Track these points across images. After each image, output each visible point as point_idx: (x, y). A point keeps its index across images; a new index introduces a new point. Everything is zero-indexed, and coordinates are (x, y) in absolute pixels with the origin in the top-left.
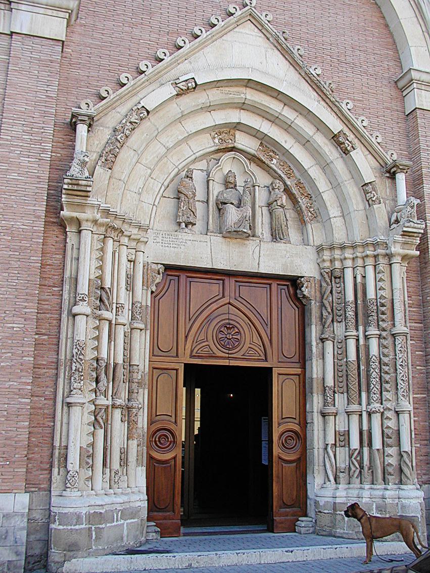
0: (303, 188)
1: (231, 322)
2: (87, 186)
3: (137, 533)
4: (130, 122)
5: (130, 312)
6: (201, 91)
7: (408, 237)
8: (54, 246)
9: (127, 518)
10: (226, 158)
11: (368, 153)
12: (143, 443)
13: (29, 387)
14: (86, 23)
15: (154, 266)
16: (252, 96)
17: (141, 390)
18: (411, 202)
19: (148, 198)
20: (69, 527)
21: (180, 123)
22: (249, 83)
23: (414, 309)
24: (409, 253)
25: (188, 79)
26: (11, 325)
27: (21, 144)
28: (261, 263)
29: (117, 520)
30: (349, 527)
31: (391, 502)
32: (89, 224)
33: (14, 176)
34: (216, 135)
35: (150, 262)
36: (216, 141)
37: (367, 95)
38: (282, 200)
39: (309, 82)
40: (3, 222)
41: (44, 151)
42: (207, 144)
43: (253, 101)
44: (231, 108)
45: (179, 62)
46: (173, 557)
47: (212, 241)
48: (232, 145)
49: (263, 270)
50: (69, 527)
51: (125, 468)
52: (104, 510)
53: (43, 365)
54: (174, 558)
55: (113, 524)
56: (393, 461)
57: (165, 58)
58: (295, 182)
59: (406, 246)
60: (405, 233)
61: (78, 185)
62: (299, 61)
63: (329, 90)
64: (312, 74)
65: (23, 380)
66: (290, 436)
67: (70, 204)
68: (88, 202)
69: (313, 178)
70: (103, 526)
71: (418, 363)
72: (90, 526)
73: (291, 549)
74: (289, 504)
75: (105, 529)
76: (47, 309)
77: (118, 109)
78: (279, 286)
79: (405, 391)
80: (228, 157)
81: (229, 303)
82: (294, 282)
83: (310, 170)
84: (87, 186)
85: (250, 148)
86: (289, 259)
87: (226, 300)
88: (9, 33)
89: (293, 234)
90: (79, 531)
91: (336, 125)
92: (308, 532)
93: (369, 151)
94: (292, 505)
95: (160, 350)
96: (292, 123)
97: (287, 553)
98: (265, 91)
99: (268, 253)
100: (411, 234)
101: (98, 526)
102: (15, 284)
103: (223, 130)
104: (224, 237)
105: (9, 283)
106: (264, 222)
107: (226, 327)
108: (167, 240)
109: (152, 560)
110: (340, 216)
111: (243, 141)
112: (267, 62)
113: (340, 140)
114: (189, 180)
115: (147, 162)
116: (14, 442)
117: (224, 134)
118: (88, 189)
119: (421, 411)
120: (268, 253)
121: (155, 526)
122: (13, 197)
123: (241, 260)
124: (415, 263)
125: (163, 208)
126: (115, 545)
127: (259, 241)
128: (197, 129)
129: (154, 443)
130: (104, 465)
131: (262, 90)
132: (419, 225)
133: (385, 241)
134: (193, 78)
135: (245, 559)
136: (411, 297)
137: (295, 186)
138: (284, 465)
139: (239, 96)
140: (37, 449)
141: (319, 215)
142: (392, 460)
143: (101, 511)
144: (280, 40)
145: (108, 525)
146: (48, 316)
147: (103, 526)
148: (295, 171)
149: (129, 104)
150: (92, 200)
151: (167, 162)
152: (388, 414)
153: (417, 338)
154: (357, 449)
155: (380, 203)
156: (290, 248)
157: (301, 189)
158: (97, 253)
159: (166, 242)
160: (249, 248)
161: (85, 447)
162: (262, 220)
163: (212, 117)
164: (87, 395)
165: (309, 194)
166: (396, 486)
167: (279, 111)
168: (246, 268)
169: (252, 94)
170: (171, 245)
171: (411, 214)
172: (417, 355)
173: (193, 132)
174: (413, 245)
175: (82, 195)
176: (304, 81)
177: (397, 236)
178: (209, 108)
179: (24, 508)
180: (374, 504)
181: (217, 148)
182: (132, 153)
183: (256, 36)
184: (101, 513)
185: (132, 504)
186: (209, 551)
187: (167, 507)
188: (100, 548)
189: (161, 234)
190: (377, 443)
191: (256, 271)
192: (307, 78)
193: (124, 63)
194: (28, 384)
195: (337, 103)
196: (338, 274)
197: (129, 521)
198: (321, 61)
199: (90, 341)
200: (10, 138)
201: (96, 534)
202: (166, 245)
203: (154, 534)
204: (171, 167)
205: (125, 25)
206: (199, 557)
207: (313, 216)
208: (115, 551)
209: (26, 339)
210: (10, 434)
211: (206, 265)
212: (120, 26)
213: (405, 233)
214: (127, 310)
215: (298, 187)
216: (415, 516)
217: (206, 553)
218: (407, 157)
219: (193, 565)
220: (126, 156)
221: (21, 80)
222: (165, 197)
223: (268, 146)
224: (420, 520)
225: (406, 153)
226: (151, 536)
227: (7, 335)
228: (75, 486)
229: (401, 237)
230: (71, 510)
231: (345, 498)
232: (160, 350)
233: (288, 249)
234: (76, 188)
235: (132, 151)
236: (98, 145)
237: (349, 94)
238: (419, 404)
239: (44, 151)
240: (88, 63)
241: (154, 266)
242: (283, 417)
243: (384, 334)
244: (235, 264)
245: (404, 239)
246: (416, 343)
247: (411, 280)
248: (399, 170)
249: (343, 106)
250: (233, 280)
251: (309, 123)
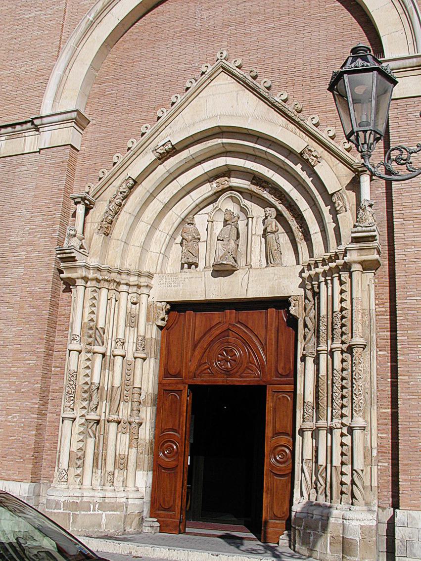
0: (294, 211)
5: (135, 345)
13: (37, 406)
17: (145, 408)
20: (50, 511)
26: (29, 362)
27: (41, 230)
28: (249, 289)
29: (94, 510)
33: (36, 253)
40: (28, 288)
41: (55, 231)
48: (228, 186)
49: (251, 295)
50: (50, 511)
53: (57, 390)
54: (118, 545)
55: (89, 513)
56: (347, 479)
57: (147, 131)
62: (265, 93)
63: (294, 111)
65: (34, 401)
70: (78, 513)
72: (69, 512)
73: (217, 553)
74: (279, 516)
75: (79, 515)
79: (357, 406)
80: (224, 198)
88: (38, 150)
90: (57, 514)
94: (282, 517)
97: (213, 556)
99: (256, 279)
101: (75, 512)
102: (32, 332)
105: (30, 332)
115: (148, 219)
116: (26, 445)
120: (256, 279)
121: (157, 521)
122: (34, 269)
126: (91, 529)
135: (175, 555)
138: (275, 477)
140: (49, 452)
144: (248, 81)
145: (82, 513)
146: (61, 353)
147: (78, 513)
150: (78, 263)
155: (346, 211)
156: (278, 271)
162: (261, 248)
166: (347, 506)
179: (25, 493)
181: (214, 191)
183: (229, 83)
184: (77, 502)
185: (118, 500)
187: (171, 507)
191: (245, 297)
194: (36, 404)
197: (108, 512)
198: (292, 85)
200: (34, 227)
201: (73, 519)
203: (149, 528)
206: (138, 547)
209: (37, 371)
210: (25, 439)
212: (119, 116)
214: (132, 344)
219: (132, 553)
221: (411, 129)
227: (26, 369)
228: (62, 480)
230: (53, 498)
233: (276, 272)
235: (128, 214)
239: (55, 231)
241: (159, 305)
244: (225, 293)
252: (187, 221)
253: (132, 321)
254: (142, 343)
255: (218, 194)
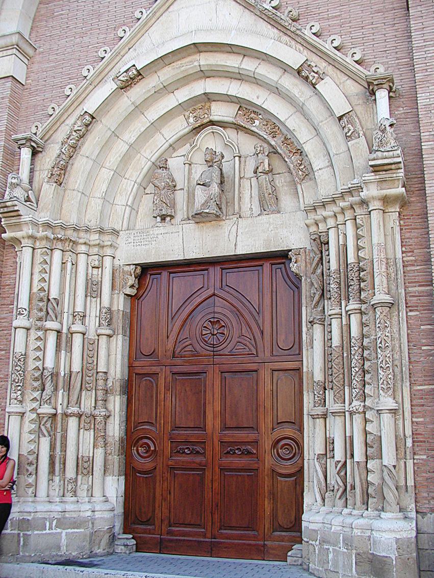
0: (291, 145)
1: (216, 315)
2: (13, 206)
3: (84, 544)
4: (75, 131)
5: (98, 319)
6: (153, 75)
7: (384, 173)
8: (12, 267)
9: (67, 526)
10: (203, 136)
11: (347, 77)
12: (114, 452)
14: (44, 50)
15: (127, 268)
16: (206, 60)
18: (382, 124)
19: (122, 199)
21: (143, 114)
22: (198, 48)
23: (418, 268)
24: (388, 193)
25: (129, 68)
29: (50, 528)
30: (319, 561)
31: (359, 534)
32: (26, 240)
34: (191, 114)
35: (121, 264)
36: (191, 120)
37: (347, 6)
38: (264, 166)
39: (266, 20)
42: (180, 126)
43: (207, 65)
44: (195, 80)
45: (122, 54)
46: (81, 571)
47: (184, 231)
49: (241, 251)
51: (91, 476)
52: (32, 517)
54: (81, 573)
55: (44, 532)
58: (282, 139)
59: (385, 185)
60: (376, 169)
61: (6, 207)
64: (266, 9)
66: (288, 444)
67: (10, 226)
68: (21, 220)
69: (291, 129)
71: (424, 341)
76: (5, 327)
77: (67, 122)
78: (273, 266)
81: (214, 295)
82: (282, 257)
83: (288, 121)
84: (13, 206)
85: (226, 116)
86: (273, 232)
87: (210, 292)
89: (287, 201)
91: (294, 57)
92: (296, 564)
93: (348, 76)
95: (291, 348)
96: (254, 74)
98: (219, 50)
100: (385, 168)
103: (197, 106)
104: (197, 223)
106: (253, 195)
107: (210, 321)
108: (138, 238)
109: (61, 573)
110: (328, 166)
111: (220, 112)
112: (217, 17)
113: (303, 74)
114: (163, 170)
117: (199, 111)
118: (16, 208)
119: (430, 408)
123: (215, 244)
124: (419, 204)
125: (145, 206)
127: (236, 219)
128: (159, 115)
129: (135, 451)
130: (52, 471)
131: (215, 49)
132: (391, 153)
133: (359, 185)
134: (134, 66)
136: (413, 252)
137: (282, 144)
139: (192, 65)
141: (308, 173)
142: (373, 478)
143: (29, 518)
145: (36, 532)
146: (5, 332)
148: (280, 128)
149: (79, 112)
151: (140, 157)
152: (369, 415)
153: (422, 306)
154: (340, 461)
157: (289, 146)
158: (40, 266)
159: (138, 241)
160: (225, 229)
161: (26, 455)
163: (175, 97)
164: (28, 404)
165: (299, 149)
167: (237, 66)
168: (221, 252)
169: (206, 57)
170: (143, 243)
171: (381, 141)
172: (423, 330)
173: (155, 120)
174: (396, 181)
175: (15, 215)
176: (262, 20)
177: (367, 175)
178: (166, 89)
180: (341, 535)
182: (85, 159)
184: (28, 520)
185: (81, 514)
186: (134, 571)
188: (27, 554)
189: (133, 233)
190: (359, 456)
191: (233, 254)
192: (263, 16)
193: (74, 75)
195: (298, 32)
196: (323, 239)
199: (32, 352)
201: (23, 540)
202: (138, 244)
203: (123, 547)
204: (143, 161)
205: (76, 37)
206: (106, 576)
207: (305, 174)
208: (48, 559)
211: (178, 257)
212: (72, 40)
213: (376, 169)
214: (94, 317)
215: (285, 144)
216: (387, 557)
217: (113, 572)
218: (409, 65)
220: (80, 166)
222: (147, 194)
223: (248, 108)
224: (394, 562)
225: (406, 60)
226: (120, 549)
229: (373, 174)
231: (321, 524)
232: (291, 348)
234: (6, 211)
235: (85, 158)
236: (48, 163)
237: (320, 14)
238: (425, 399)
240: (44, 86)
241: (127, 268)
242: (279, 422)
243: (364, 307)
245: (377, 177)
246: (422, 314)
247: (413, 229)
248: (376, 88)
249: (306, 33)
250: (218, 268)
251: (274, 67)
252: (161, 165)
253: (93, 289)
254: (108, 317)
255: (197, 130)
